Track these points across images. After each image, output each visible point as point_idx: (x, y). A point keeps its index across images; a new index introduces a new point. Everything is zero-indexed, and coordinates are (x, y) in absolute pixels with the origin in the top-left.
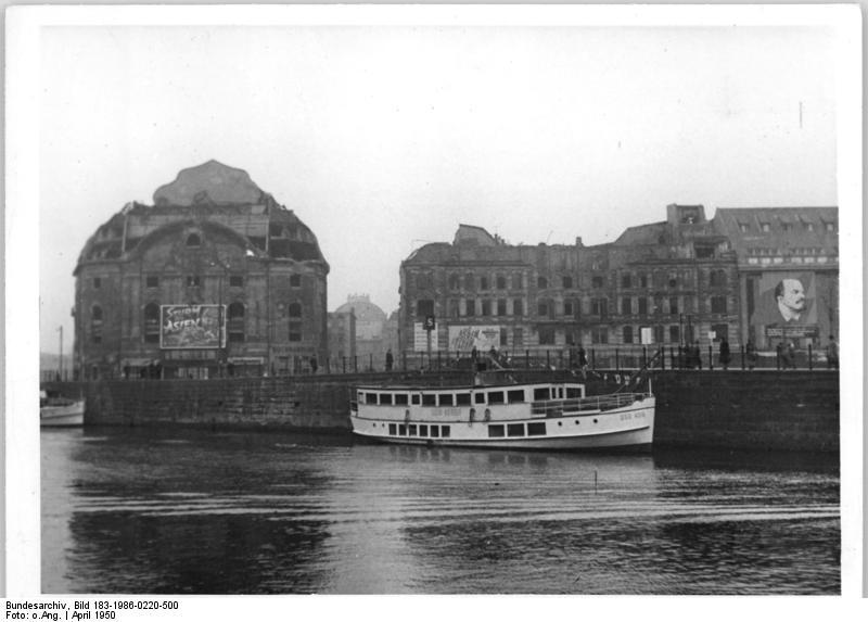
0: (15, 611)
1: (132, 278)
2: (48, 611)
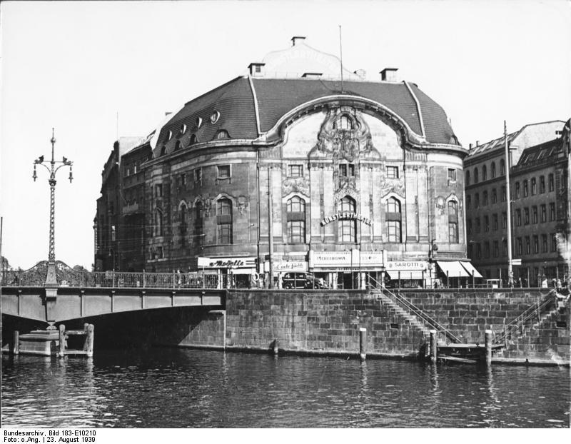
0: (10, 437)
1: (271, 166)
2: (32, 437)
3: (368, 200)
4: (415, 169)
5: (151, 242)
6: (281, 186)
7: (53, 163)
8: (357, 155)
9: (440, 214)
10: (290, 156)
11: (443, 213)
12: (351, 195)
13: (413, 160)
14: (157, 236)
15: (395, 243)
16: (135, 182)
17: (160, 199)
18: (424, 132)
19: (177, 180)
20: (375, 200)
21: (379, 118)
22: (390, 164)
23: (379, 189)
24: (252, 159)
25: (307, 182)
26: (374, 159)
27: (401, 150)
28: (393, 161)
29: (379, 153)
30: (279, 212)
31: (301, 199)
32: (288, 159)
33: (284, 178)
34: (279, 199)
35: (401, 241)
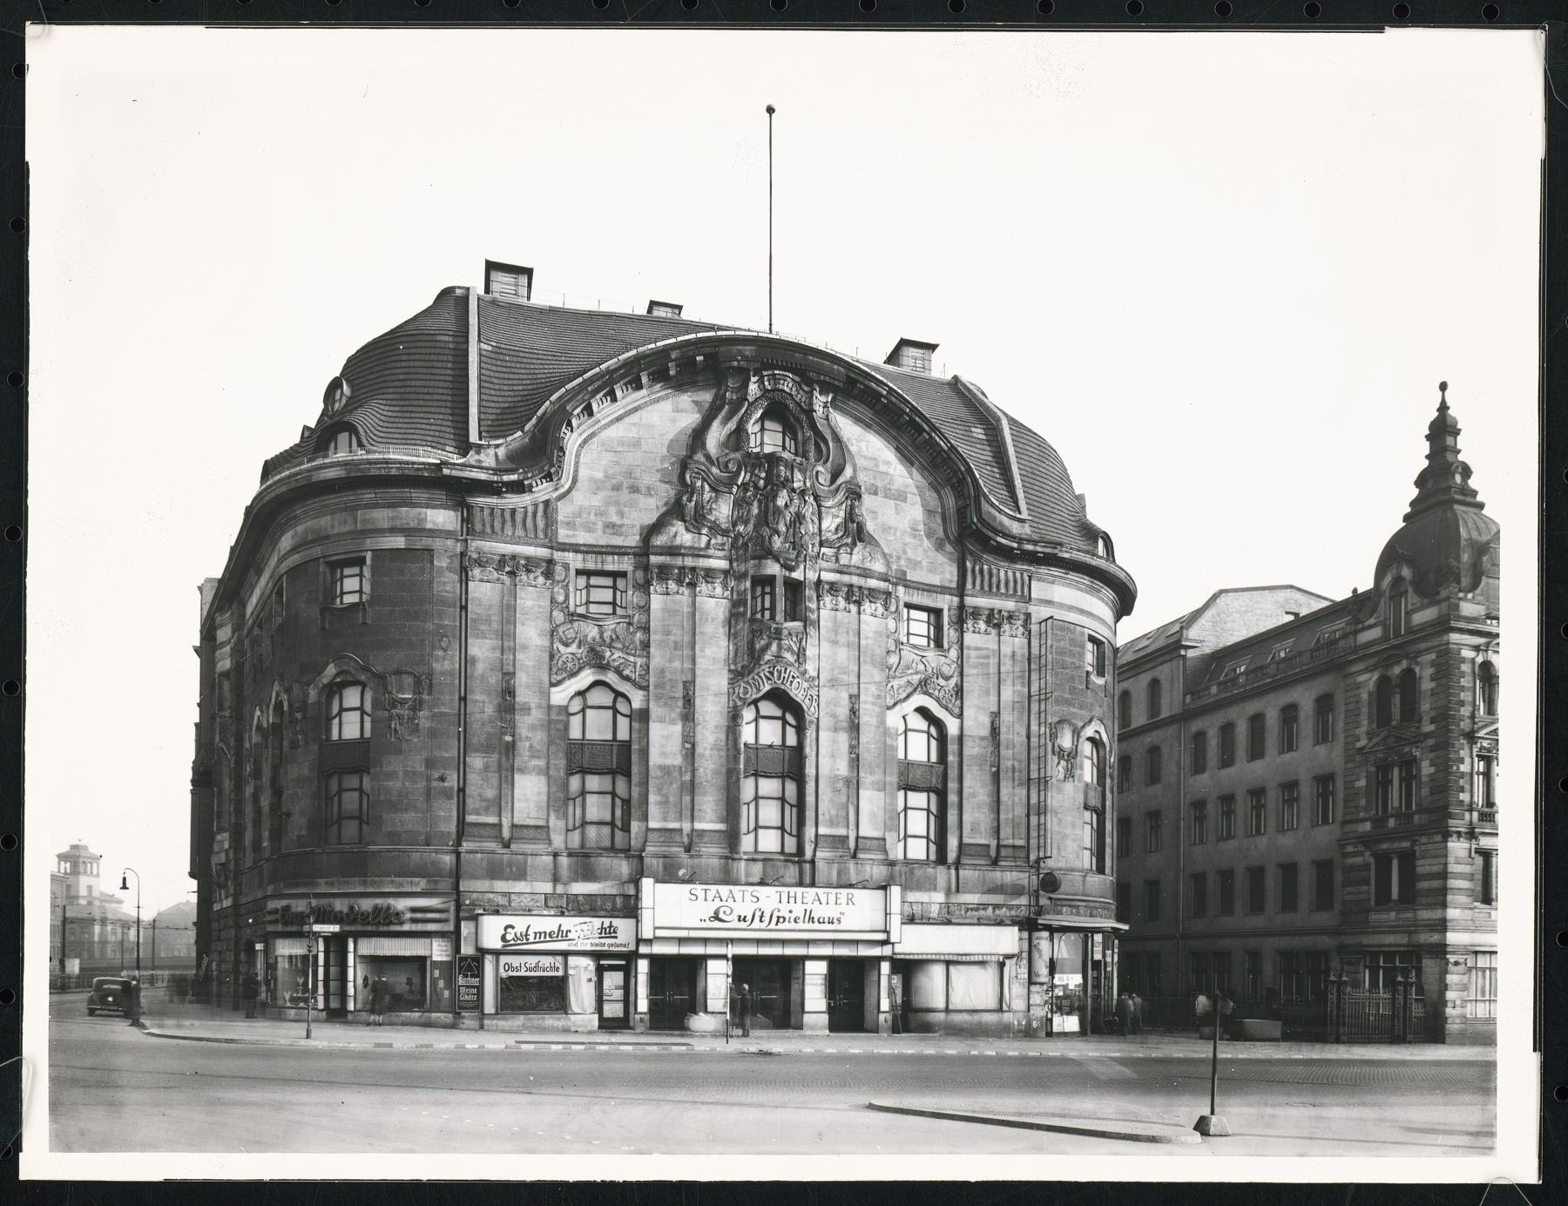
1: (511, 567)
3: (843, 711)
4: (995, 620)
6: (547, 643)
8: (812, 550)
9: (1061, 776)
10: (582, 538)
20: (867, 718)
22: (917, 598)
24: (448, 534)
26: (866, 573)
28: (930, 589)
30: (539, 738)
31: (618, 694)
32: (575, 548)
33: (559, 616)
35: (941, 859)
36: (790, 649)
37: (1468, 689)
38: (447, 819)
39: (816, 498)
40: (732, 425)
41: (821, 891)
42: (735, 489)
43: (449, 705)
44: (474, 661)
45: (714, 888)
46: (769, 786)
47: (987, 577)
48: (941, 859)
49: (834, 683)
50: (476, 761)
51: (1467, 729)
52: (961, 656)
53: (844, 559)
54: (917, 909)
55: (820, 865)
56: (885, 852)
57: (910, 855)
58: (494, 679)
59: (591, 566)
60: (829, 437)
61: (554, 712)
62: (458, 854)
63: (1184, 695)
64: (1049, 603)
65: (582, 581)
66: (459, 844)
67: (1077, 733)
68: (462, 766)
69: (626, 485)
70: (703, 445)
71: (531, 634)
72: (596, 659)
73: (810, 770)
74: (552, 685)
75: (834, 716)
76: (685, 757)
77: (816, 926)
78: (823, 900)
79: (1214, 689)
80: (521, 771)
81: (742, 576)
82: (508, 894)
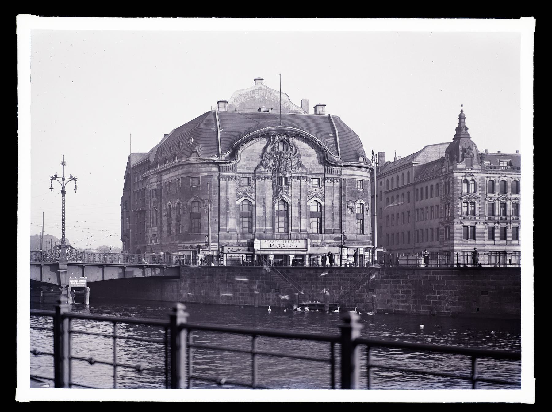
1: (228, 177)
3: (297, 203)
4: (332, 180)
5: (150, 231)
7: (63, 179)
8: (290, 169)
10: (242, 171)
11: (352, 212)
12: (285, 199)
13: (331, 174)
14: (153, 226)
15: (316, 233)
16: (141, 187)
17: (155, 199)
18: (339, 153)
19: (166, 186)
20: (302, 203)
21: (307, 143)
23: (305, 195)
24: (215, 172)
25: (254, 190)
26: (302, 173)
27: (321, 167)
28: (317, 174)
29: (306, 169)
30: (234, 211)
32: (241, 173)
33: (238, 187)
34: (234, 201)
36: (285, 191)
37: (460, 186)
38: (217, 228)
39: (290, 159)
40: (273, 146)
41: (292, 240)
42: (273, 159)
43: (216, 206)
44: (221, 197)
45: (270, 240)
46: (281, 219)
47: (330, 171)
48: (321, 233)
49: (295, 197)
50: (222, 216)
51: (460, 197)
52: (325, 188)
53: (297, 171)
54: (315, 244)
55: (292, 235)
56: (307, 232)
57: (313, 232)
58: (225, 200)
59: (244, 176)
60: (293, 146)
61: (237, 206)
62: (219, 235)
63: (414, 178)
64: (346, 175)
65: (242, 178)
66: (219, 233)
67: (354, 203)
68: (219, 217)
69: (250, 159)
70: (266, 151)
71: (232, 191)
72: (245, 195)
73: (290, 216)
74: (236, 200)
75: (295, 204)
76: (263, 214)
77: (292, 248)
78: (293, 242)
79: (420, 177)
80: (231, 218)
81: (275, 177)
82: (228, 242)
